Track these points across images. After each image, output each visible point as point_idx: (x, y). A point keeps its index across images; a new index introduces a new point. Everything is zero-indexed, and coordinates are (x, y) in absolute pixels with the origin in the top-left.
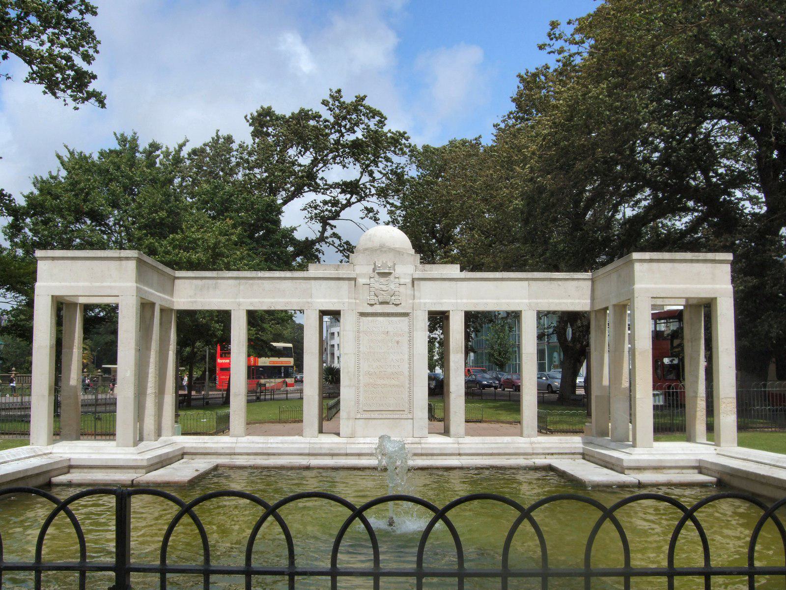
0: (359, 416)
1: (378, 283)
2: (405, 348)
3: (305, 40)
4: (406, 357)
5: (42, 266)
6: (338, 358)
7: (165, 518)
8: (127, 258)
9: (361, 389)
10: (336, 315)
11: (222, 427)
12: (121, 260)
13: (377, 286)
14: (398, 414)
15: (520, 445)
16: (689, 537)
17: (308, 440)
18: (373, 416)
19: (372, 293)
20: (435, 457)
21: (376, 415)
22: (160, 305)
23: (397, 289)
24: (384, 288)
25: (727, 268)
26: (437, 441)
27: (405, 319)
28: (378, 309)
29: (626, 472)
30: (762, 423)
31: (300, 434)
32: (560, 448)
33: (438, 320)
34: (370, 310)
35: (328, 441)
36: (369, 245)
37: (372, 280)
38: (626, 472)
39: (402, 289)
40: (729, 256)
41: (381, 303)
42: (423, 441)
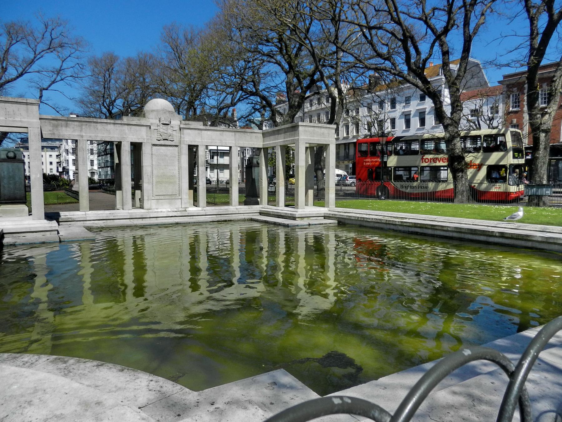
0: (153, 198)
1: (162, 129)
2: (60, 122)
3: (539, 403)
4: (177, 168)
6: (426, 240)
9: (154, 184)
12: (27, 105)
13: (161, 130)
18: (161, 198)
21: (162, 197)
23: (171, 133)
24: (165, 132)
26: (193, 209)
27: (176, 148)
28: (162, 142)
29: (297, 219)
30: (272, 180)
31: (78, 210)
32: (302, 214)
36: (155, 108)
37: (159, 127)
38: (297, 219)
39: (174, 133)
41: (164, 140)
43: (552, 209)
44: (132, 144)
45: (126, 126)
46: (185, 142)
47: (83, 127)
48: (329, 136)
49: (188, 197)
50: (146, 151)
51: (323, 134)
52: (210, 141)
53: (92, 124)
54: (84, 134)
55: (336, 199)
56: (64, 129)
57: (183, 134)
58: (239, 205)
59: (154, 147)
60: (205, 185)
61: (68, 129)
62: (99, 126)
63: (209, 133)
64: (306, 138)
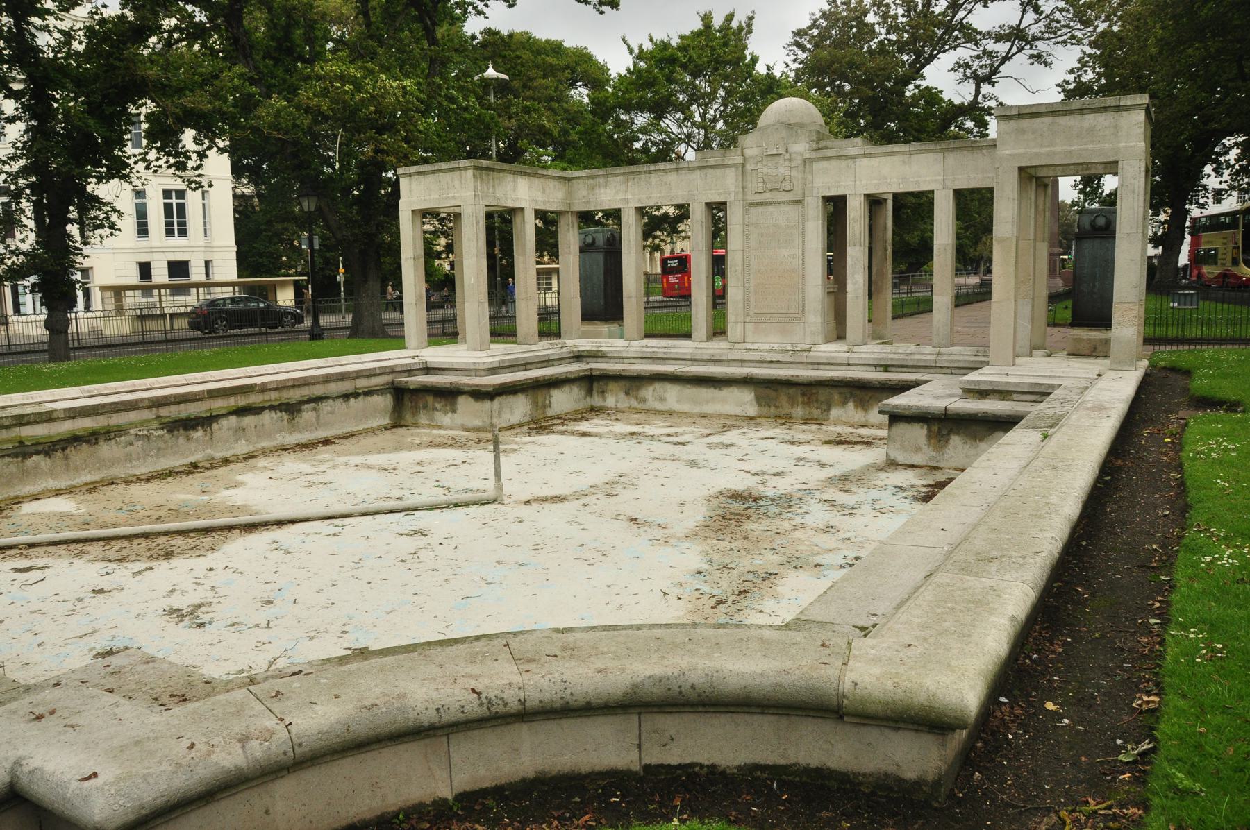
5: (404, 183)
7: (425, 439)
8: (465, 168)
10: (722, 206)
11: (392, 336)
14: (790, 319)
15: (864, 356)
16: (731, 506)
17: (411, 353)
19: (761, 180)
20: (822, 367)
22: (640, 210)
25: (1141, 116)
28: (768, 197)
31: (403, 347)
33: (836, 207)
34: (758, 198)
35: (718, 347)
40: (1144, 99)
42: (856, 349)
43: (120, 360)
44: (827, 199)
45: (698, 172)
46: (815, 191)
47: (630, 184)
48: (1116, 135)
49: (819, 319)
50: (735, 218)
51: (1092, 130)
52: (875, 182)
53: (643, 176)
54: (630, 197)
55: (429, 335)
56: (602, 191)
57: (812, 173)
58: (430, 344)
59: (753, 210)
60: (424, 315)
61: (609, 191)
62: (653, 178)
63: (874, 161)
64: (1022, 151)
